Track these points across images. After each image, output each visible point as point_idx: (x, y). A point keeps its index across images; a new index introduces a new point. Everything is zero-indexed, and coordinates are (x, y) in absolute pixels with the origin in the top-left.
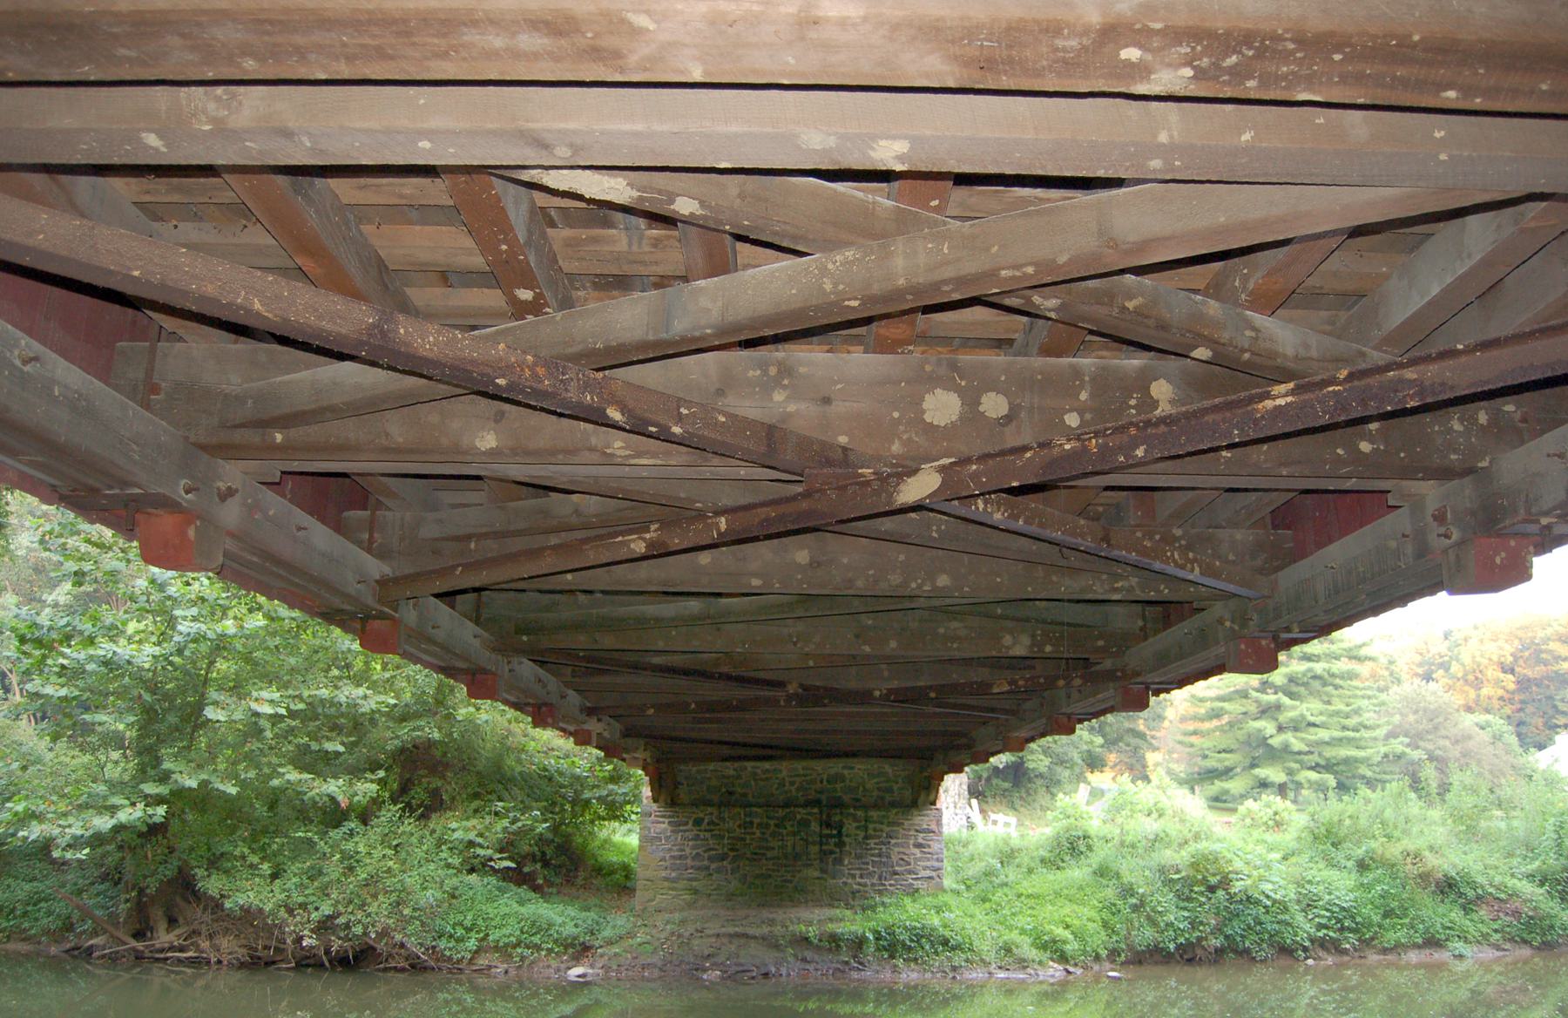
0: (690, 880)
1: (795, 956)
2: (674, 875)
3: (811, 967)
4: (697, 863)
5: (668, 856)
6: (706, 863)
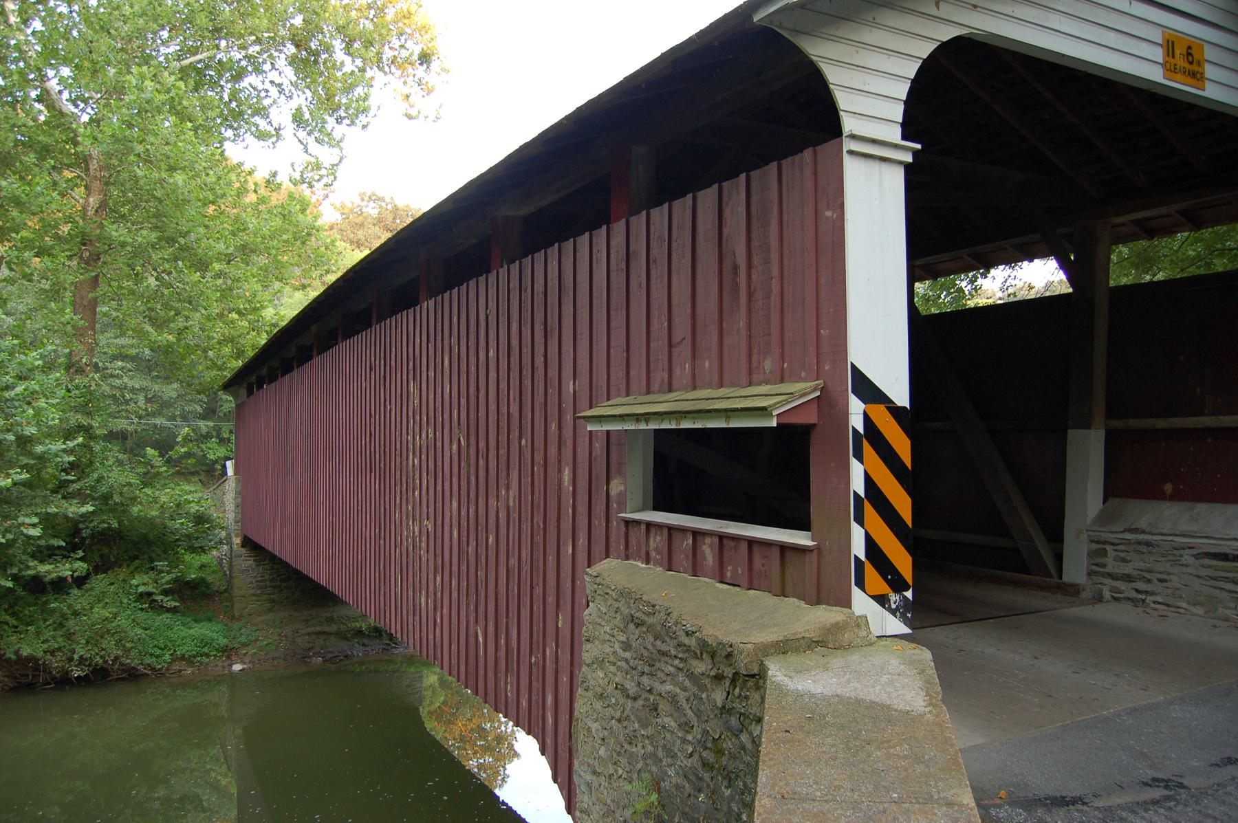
0: (269, 594)
1: (358, 643)
2: (258, 592)
3: (369, 649)
4: (273, 584)
5: (254, 581)
6: (279, 583)
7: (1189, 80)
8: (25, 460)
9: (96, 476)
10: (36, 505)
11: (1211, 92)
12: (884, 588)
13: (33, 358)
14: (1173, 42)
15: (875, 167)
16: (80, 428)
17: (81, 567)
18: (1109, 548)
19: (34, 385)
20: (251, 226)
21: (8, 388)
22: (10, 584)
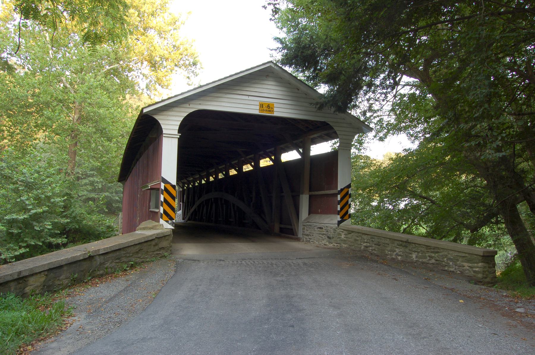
7: (266, 112)
8: (48, 204)
9: (72, 210)
10: (51, 219)
11: (276, 114)
12: (168, 219)
13: (52, 170)
14: (263, 104)
15: (170, 139)
16: (67, 194)
17: (65, 240)
18: (305, 227)
19: (51, 179)
20: (128, 125)
21: (43, 180)
22: (41, 244)
